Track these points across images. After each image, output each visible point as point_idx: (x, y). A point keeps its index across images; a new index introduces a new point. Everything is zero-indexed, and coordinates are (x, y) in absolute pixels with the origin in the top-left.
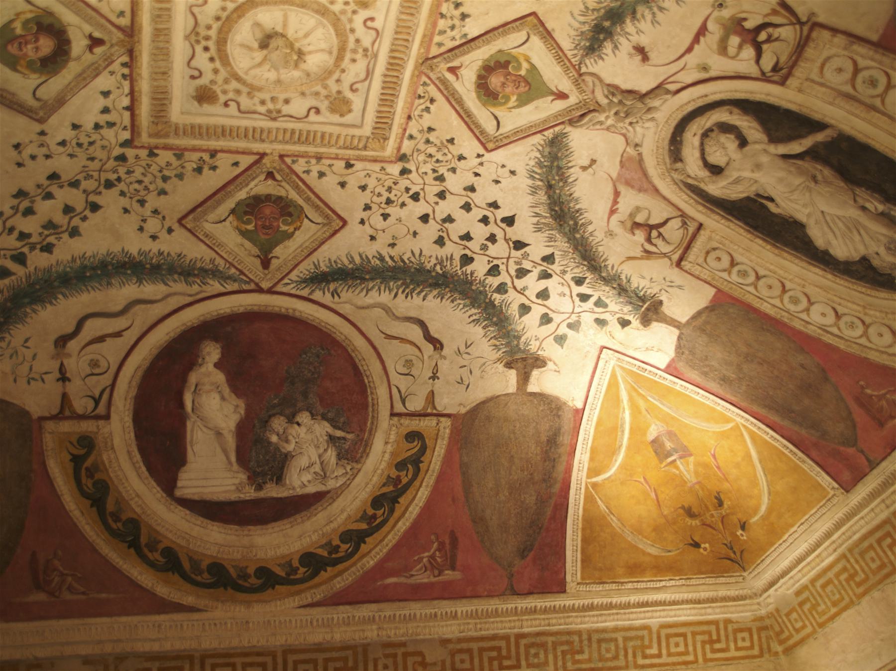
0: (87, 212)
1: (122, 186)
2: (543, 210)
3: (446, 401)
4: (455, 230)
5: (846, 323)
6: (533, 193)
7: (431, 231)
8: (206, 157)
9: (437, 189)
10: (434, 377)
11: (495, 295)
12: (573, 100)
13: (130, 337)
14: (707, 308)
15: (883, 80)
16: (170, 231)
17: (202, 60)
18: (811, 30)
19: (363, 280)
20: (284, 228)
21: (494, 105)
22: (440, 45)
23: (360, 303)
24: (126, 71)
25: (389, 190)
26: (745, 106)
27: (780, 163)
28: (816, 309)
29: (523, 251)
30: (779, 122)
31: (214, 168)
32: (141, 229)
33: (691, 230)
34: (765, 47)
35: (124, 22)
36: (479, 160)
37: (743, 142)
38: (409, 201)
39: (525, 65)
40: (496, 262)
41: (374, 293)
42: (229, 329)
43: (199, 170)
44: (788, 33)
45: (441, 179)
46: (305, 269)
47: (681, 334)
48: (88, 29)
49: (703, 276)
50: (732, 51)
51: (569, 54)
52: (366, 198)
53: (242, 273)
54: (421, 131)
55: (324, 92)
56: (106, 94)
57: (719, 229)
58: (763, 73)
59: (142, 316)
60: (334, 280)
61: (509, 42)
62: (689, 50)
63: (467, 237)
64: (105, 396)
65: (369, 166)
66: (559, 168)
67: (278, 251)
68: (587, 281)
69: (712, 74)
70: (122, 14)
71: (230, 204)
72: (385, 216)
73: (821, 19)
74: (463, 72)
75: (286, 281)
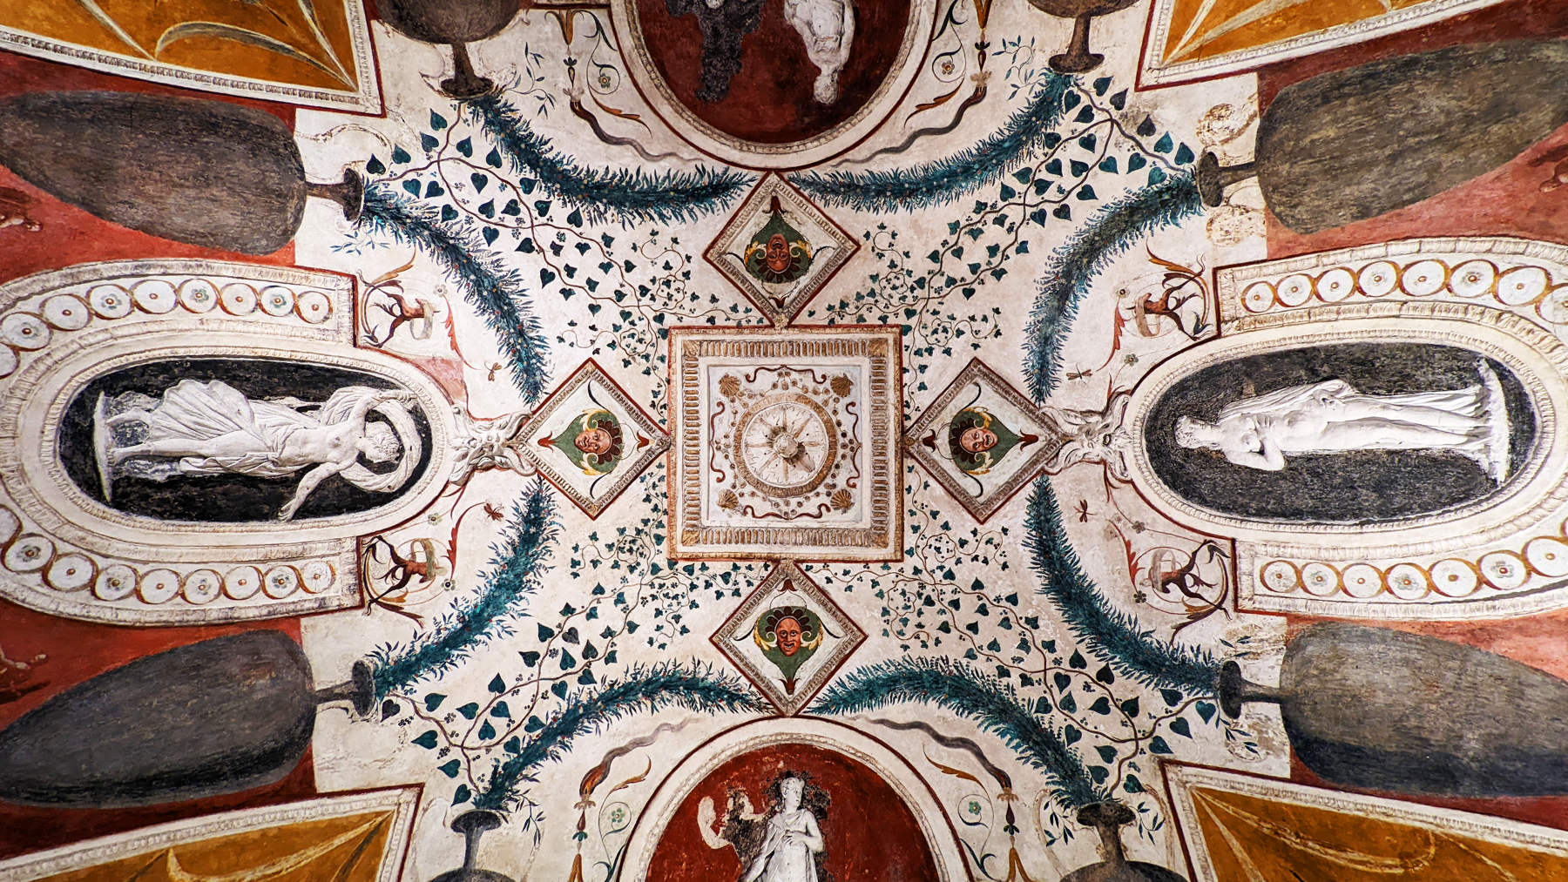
0: (941, 250)
1: (910, 281)
2: (519, 301)
3: (548, 28)
4: (595, 256)
5: (120, 303)
6: (534, 320)
7: (620, 253)
8: (838, 320)
9: (625, 302)
10: (571, 63)
11: (532, 177)
12: (534, 441)
13: (909, 105)
14: (293, 233)
15: (271, 590)
16: (867, 235)
17: (847, 422)
18: (362, 599)
19: (675, 190)
20: (762, 247)
21: (599, 414)
22: (660, 466)
23: (674, 160)
24: (907, 411)
25: (670, 297)
26: (381, 499)
27: (314, 458)
28: (168, 299)
29: (522, 238)
30: (339, 498)
31: (830, 308)
32: (894, 235)
33: (362, 332)
34: (393, 565)
35: (908, 462)
36: (596, 346)
37: (362, 459)
38: (649, 285)
39: (585, 464)
40: (544, 220)
41: (662, 174)
42: (807, 120)
43: (843, 305)
44: (379, 587)
45: (625, 315)
46: (736, 202)
47: (303, 178)
48: (935, 455)
49: (320, 276)
50: (418, 547)
51: (554, 489)
52: (691, 287)
53: (797, 191)
54: (655, 368)
55: (745, 399)
56: (922, 387)
57: (335, 351)
58: (381, 538)
59: (893, 134)
60: (704, 188)
61: (608, 482)
62: (455, 532)
63: (583, 248)
64: (940, 24)
65: (693, 322)
66: (520, 360)
67: (765, 220)
68: (440, 217)
69: (424, 517)
70: (911, 469)
71: (815, 269)
72: (667, 266)
73: (360, 612)
74: (635, 442)
75: (753, 184)
